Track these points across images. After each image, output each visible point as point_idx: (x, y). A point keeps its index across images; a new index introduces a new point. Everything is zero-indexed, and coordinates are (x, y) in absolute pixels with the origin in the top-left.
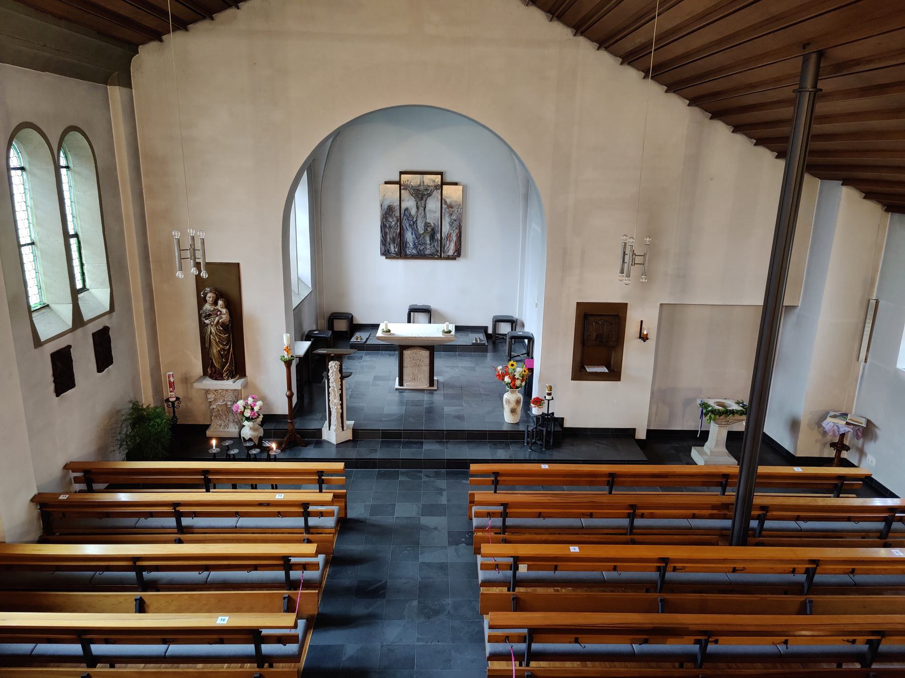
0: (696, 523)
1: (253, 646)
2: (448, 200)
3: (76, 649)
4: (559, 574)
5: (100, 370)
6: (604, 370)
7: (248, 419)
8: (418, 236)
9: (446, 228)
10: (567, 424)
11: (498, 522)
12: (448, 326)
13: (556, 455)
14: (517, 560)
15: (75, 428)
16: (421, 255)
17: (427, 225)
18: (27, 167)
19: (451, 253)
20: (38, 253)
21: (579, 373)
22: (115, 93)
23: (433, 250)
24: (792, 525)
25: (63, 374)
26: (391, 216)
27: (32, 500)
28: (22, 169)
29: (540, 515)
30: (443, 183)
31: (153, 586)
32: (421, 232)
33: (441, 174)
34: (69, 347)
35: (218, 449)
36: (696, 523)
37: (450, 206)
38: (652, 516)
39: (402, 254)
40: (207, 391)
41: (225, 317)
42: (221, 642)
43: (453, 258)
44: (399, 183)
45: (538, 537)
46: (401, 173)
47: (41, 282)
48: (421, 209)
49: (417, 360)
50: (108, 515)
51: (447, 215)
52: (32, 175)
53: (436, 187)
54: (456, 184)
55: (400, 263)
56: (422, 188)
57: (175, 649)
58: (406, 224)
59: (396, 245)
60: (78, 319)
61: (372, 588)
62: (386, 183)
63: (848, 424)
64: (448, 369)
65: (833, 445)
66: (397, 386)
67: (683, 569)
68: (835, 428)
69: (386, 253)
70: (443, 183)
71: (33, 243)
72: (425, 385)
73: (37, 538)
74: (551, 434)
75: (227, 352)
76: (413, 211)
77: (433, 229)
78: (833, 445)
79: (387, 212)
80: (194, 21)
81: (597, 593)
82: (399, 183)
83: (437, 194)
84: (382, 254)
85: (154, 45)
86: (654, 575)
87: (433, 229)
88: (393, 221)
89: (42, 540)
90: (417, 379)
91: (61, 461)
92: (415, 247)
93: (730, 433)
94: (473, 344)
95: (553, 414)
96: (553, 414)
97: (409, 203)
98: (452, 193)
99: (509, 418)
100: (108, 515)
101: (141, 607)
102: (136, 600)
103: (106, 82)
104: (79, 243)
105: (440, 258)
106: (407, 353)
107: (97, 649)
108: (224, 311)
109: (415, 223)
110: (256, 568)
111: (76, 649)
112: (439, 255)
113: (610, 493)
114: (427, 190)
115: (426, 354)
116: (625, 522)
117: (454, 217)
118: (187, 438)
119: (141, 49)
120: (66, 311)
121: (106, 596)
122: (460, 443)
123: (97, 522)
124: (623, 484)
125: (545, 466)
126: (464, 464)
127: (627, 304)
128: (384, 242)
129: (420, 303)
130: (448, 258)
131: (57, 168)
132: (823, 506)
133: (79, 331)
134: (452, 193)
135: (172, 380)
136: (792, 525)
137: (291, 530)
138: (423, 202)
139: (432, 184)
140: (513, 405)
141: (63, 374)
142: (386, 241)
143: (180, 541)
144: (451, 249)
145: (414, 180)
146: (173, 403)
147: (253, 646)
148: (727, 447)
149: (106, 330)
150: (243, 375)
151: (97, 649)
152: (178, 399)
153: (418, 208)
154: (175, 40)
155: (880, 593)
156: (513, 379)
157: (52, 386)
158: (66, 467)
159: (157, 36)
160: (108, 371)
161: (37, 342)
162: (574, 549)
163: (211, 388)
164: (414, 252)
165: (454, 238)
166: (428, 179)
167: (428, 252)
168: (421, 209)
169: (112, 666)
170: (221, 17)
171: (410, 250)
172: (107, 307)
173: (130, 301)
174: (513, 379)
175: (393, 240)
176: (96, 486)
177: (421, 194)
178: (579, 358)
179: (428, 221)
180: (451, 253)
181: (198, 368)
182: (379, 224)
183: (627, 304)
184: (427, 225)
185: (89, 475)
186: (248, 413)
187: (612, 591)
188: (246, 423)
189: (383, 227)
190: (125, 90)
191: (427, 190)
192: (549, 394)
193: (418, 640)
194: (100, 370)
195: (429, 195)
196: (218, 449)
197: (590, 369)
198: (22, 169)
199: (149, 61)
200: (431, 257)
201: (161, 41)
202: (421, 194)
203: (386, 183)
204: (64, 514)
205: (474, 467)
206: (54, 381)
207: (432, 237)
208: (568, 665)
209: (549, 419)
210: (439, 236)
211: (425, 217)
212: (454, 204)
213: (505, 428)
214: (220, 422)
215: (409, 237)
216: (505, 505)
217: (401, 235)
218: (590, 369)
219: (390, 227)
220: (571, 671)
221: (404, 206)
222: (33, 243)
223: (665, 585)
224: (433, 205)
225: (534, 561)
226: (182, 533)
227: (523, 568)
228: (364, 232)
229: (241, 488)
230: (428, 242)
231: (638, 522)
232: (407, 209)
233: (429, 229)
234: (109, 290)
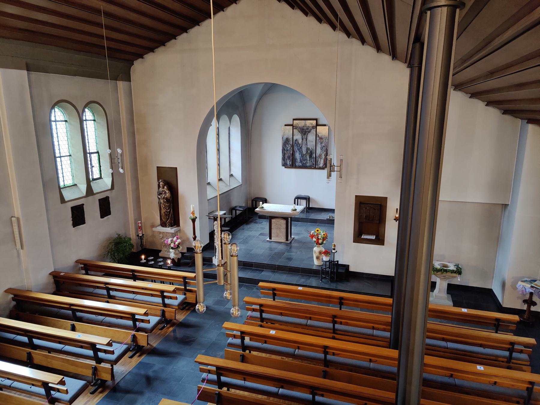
0: (376, 332)
1: (311, 396)
2: (320, 135)
3: (25, 339)
4: (265, 346)
5: (102, 217)
6: (373, 237)
7: (172, 248)
8: (302, 155)
9: (319, 151)
10: (351, 269)
11: (257, 314)
12: (294, 207)
13: (340, 286)
14: (243, 334)
15: (86, 242)
16: (304, 167)
17: (308, 149)
18: (68, 120)
19: (321, 165)
20: (73, 160)
21: (358, 238)
22: (121, 84)
23: (311, 164)
24: (443, 344)
25: (78, 216)
26: (288, 144)
27: (50, 274)
28: (66, 121)
29: (281, 314)
30: (317, 125)
31: (80, 320)
32: (304, 153)
33: (316, 120)
34: (83, 204)
35: (145, 261)
36: (376, 332)
37: (321, 138)
38: (347, 324)
39: (293, 166)
40: (160, 233)
41: (168, 195)
42: (82, 347)
43: (323, 168)
44: (292, 125)
45: (295, 329)
46: (294, 120)
47: (67, 174)
48: (304, 140)
49: (279, 226)
50: (81, 285)
51: (319, 143)
52: (70, 124)
53: (313, 127)
54: (325, 125)
55: (293, 171)
56: (305, 128)
57: (68, 348)
58: (296, 148)
59: (291, 160)
60: (90, 192)
61: (187, 340)
62: (286, 125)
63: (532, 287)
64: (299, 232)
65: (525, 301)
66: (268, 239)
67: (338, 355)
68: (524, 289)
69: (285, 165)
70: (317, 125)
71: (70, 156)
72: (283, 240)
73: (52, 292)
74: (338, 274)
75: (171, 214)
76: (300, 141)
77: (311, 152)
78: (525, 301)
79: (286, 142)
80: (157, 47)
81: (305, 364)
82: (292, 125)
83: (313, 131)
84: (283, 165)
85: (140, 60)
86: (238, 341)
87: (311, 152)
88: (289, 147)
89: (54, 294)
90: (279, 236)
91: (75, 258)
92: (301, 161)
93: (448, 284)
94: (328, 220)
95: (338, 261)
96: (338, 261)
97: (298, 136)
98: (322, 131)
99: (316, 262)
100: (81, 285)
101: (73, 329)
102: (241, 355)
103: (116, 80)
104: (99, 156)
105: (315, 168)
106: (273, 220)
107: (36, 341)
108: (167, 191)
109: (301, 148)
110: (121, 318)
111: (25, 339)
112: (314, 166)
113: (340, 309)
114: (308, 129)
115: (284, 222)
116: (331, 325)
117: (323, 145)
118: (154, 255)
119: (135, 62)
120: (83, 188)
121: (92, 327)
122: (282, 273)
123: (91, 290)
124: (280, 295)
125: (300, 288)
126: (255, 282)
127: (387, 198)
128: (284, 159)
129: (303, 194)
130: (320, 168)
131: (81, 121)
132: (457, 333)
133: (90, 198)
134: (322, 131)
135: (140, 225)
136: (443, 344)
137: (325, 329)
138: (306, 136)
139: (310, 126)
140: (318, 254)
141: (78, 216)
142: (285, 158)
143: (108, 302)
144: (321, 163)
145: (301, 123)
146: (141, 237)
147: (311, 396)
148: (448, 293)
149: (107, 198)
150: (178, 225)
151: (36, 341)
152: (143, 235)
153: (302, 140)
154: (149, 57)
155: (468, 393)
156: (318, 239)
157: (71, 222)
158: (78, 262)
159: (141, 56)
160: (108, 218)
161: (63, 200)
162: (273, 332)
163: (162, 231)
164: (300, 164)
165: (323, 157)
166: (308, 123)
167: (308, 165)
168: (304, 140)
169: (49, 353)
170: (168, 44)
171: (298, 163)
172: (110, 187)
173: (125, 184)
174: (318, 239)
175: (289, 157)
176: (89, 272)
177: (305, 132)
178: (357, 230)
179: (308, 147)
180: (321, 165)
181: (158, 221)
182: (281, 148)
183: (387, 198)
184: (308, 149)
185: (88, 267)
186: (172, 245)
187: (314, 365)
188: (171, 250)
189: (283, 150)
190: (126, 83)
191: (308, 129)
192: (334, 249)
193: (192, 369)
194: (102, 217)
195: (309, 132)
196: (145, 261)
197: (364, 237)
198: (66, 121)
199: (139, 68)
200: (310, 167)
201: (143, 58)
202: (305, 132)
203: (286, 125)
204: (64, 282)
205: (261, 284)
206: (72, 220)
207: (311, 156)
208: (260, 396)
209: (334, 264)
210: (314, 155)
211: (307, 144)
212: (323, 137)
213: (314, 268)
214: (166, 249)
215: (298, 156)
216: (261, 305)
217: (293, 154)
218: (364, 237)
219: (287, 150)
220: (240, 396)
221: (295, 138)
222: (70, 156)
223: (327, 363)
224: (311, 137)
225: (253, 336)
226: (110, 298)
227: (247, 339)
228: (273, 153)
229: (92, 273)
230: (308, 159)
231: (337, 326)
232: (296, 140)
233: (309, 152)
234: (111, 179)
